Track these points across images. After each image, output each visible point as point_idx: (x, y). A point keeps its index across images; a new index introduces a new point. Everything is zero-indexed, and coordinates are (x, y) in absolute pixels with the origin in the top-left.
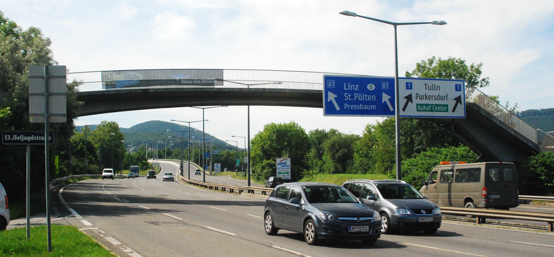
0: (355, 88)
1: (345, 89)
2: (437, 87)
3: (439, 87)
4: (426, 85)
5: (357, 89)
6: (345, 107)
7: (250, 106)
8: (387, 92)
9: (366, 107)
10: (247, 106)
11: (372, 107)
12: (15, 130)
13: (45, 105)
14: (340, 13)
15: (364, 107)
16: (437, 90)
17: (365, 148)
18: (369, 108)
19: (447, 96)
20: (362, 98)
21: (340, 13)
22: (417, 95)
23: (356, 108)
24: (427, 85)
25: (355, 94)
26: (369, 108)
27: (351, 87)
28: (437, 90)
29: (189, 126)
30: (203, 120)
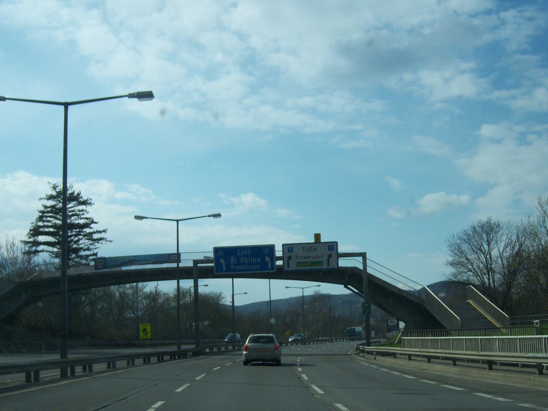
0: (248, 253)
1: (239, 254)
2: (314, 249)
3: (316, 250)
4: (303, 248)
5: (250, 253)
6: (232, 267)
7: (234, 279)
8: (268, 256)
9: (251, 267)
10: (231, 279)
11: (257, 266)
12: (241, 338)
13: (546, 359)
14: (80, 190)
15: (249, 267)
16: (314, 252)
17: (18, 262)
18: (253, 267)
19: (323, 256)
20: (247, 260)
21: (80, 190)
22: (297, 257)
23: (242, 269)
24: (304, 248)
25: (242, 258)
26: (253, 267)
27: (244, 252)
28: (314, 252)
29: (231, 304)
30: (235, 296)
